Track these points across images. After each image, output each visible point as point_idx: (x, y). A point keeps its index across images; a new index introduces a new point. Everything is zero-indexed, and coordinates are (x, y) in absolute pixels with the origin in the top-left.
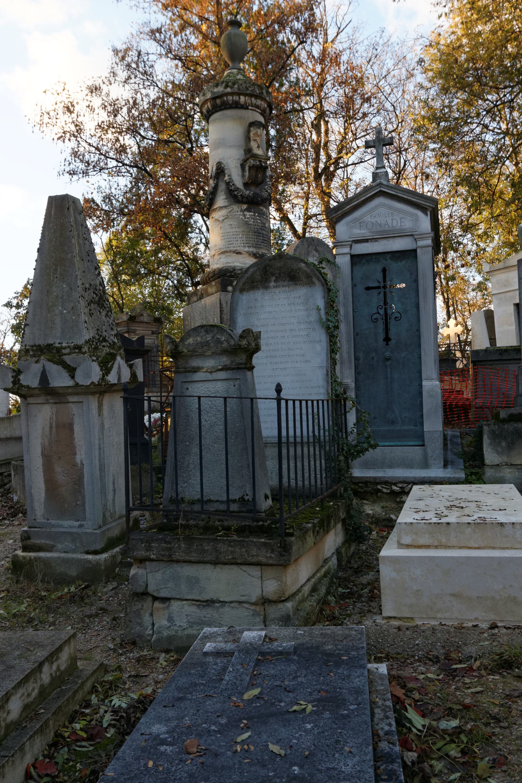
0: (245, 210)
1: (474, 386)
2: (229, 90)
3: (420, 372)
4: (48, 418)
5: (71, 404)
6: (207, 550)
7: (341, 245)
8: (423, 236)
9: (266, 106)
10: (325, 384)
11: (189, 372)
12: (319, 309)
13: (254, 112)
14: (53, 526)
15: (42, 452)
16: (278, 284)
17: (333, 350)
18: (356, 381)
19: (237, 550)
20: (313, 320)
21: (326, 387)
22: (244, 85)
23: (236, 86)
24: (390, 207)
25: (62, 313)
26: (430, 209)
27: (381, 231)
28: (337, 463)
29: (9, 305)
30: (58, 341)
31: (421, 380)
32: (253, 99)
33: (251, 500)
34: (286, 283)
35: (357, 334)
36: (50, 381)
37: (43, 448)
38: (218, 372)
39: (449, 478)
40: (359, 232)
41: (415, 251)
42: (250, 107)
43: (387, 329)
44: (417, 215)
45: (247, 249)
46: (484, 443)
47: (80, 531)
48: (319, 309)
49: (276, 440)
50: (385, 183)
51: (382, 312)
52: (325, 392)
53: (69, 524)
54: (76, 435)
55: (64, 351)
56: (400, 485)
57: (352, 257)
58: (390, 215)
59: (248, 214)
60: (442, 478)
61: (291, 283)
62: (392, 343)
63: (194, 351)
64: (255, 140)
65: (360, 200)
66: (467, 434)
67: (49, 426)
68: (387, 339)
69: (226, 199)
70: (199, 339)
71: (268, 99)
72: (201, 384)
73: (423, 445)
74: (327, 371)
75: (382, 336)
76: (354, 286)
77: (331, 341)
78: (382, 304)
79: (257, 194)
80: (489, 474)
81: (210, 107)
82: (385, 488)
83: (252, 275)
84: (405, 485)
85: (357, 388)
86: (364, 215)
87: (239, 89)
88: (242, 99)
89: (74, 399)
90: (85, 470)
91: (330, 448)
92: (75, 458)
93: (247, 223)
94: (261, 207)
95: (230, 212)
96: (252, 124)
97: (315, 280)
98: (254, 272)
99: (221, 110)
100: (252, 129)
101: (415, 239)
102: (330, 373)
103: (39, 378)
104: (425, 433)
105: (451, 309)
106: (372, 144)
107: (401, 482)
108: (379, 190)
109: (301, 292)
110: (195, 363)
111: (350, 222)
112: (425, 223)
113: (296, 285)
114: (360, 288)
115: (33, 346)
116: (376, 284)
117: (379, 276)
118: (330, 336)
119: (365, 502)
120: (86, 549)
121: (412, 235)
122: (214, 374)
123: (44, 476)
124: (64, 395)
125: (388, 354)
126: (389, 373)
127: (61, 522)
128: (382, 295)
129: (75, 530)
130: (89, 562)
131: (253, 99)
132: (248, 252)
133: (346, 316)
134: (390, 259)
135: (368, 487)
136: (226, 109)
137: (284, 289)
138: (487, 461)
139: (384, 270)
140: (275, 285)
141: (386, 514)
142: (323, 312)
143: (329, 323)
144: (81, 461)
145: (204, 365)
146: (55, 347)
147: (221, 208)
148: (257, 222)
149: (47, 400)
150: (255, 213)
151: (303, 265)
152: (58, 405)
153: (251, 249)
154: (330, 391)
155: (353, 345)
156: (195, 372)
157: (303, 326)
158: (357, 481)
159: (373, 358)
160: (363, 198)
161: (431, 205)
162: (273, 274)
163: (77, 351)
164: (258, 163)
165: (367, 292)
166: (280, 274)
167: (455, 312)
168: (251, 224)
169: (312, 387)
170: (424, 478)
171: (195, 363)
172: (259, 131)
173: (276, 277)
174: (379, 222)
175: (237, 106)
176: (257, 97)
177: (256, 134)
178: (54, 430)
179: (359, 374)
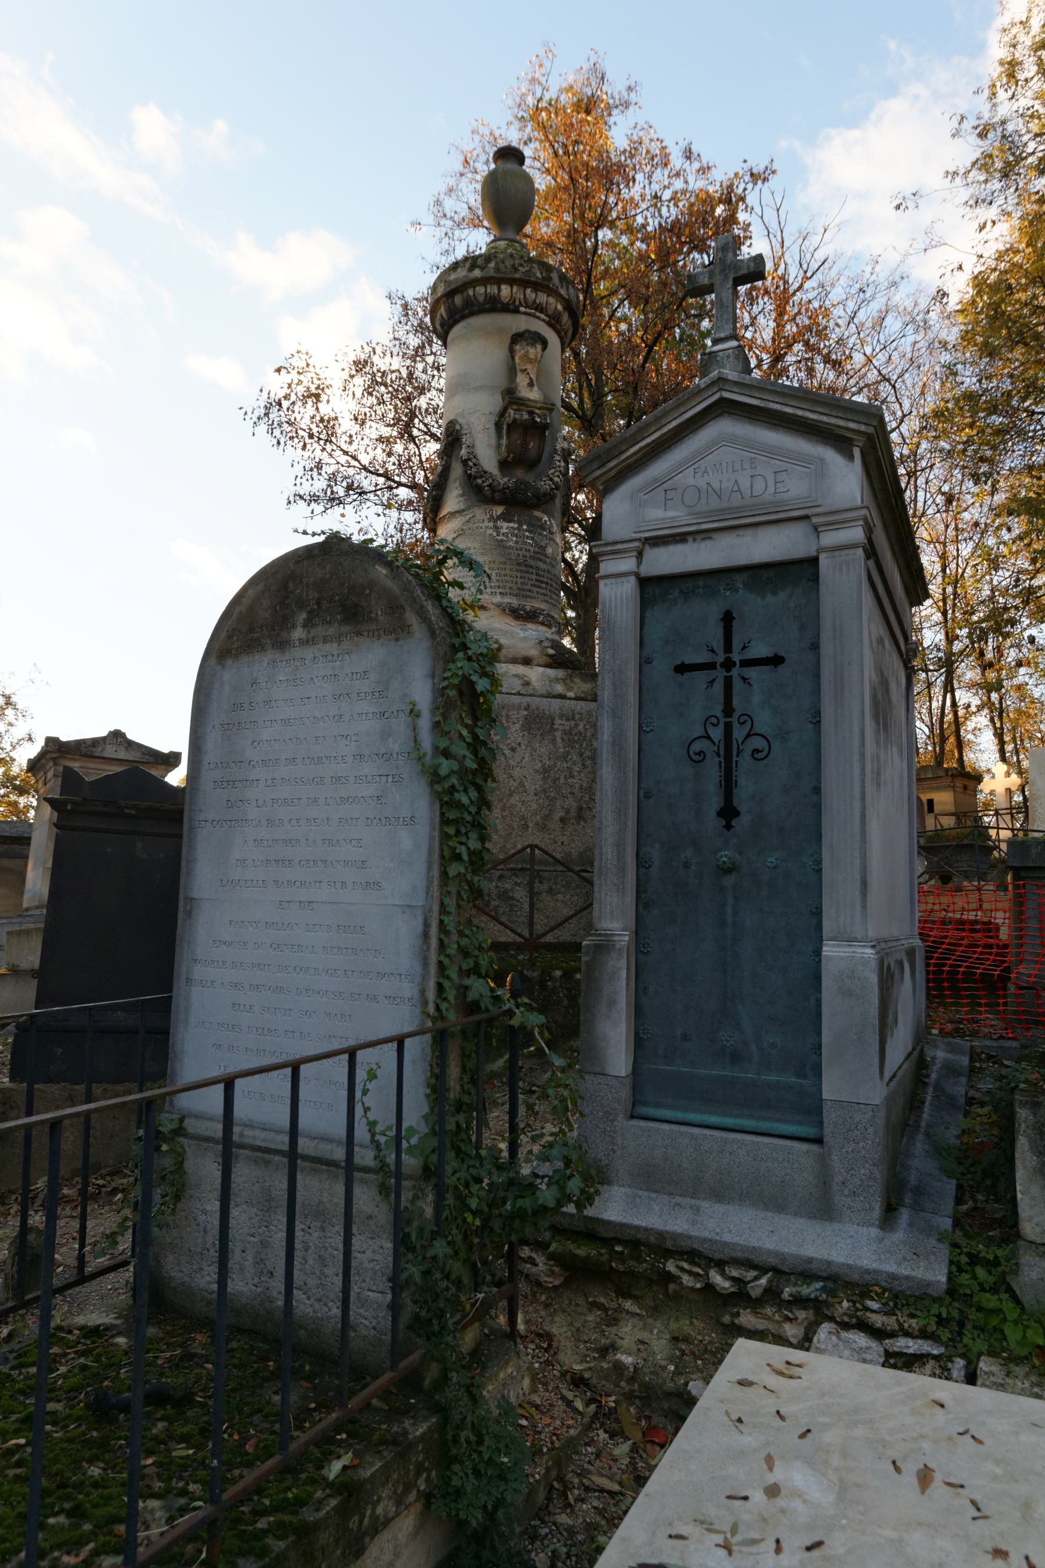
0: (499, 518)
1: (1017, 929)
2: (477, 273)
3: (817, 913)
7: (613, 552)
8: (837, 519)
9: (560, 307)
10: (418, 969)
12: (414, 713)
13: (532, 319)
21: (418, 979)
22: (509, 263)
23: (492, 265)
24: (748, 445)
26: (861, 441)
27: (722, 510)
31: (821, 939)
32: (528, 291)
34: (332, 631)
35: (647, 796)
39: (893, 1277)
40: (661, 515)
41: (813, 562)
42: (522, 309)
43: (728, 785)
44: (822, 460)
45: (498, 599)
46: (1019, 1164)
48: (414, 713)
50: (731, 374)
51: (717, 734)
56: (735, 1273)
58: (747, 466)
59: (504, 526)
60: (868, 1272)
61: (345, 629)
62: (743, 822)
64: (523, 371)
65: (665, 430)
66: (990, 1057)
68: (728, 813)
69: (462, 495)
71: (563, 292)
73: (819, 1141)
74: (427, 925)
75: (714, 802)
76: (644, 662)
78: (718, 711)
79: (526, 484)
80: (1034, 1275)
82: (690, 1273)
84: (753, 1273)
86: (678, 470)
87: (497, 269)
88: (505, 290)
93: (500, 545)
94: (536, 513)
95: (468, 521)
96: (517, 338)
99: (464, 317)
101: (816, 528)
102: (434, 931)
104: (826, 1107)
105: (1009, 747)
106: (705, 280)
107: (737, 1262)
108: (717, 396)
109: (371, 655)
111: (640, 490)
112: (846, 481)
113: (359, 634)
114: (662, 668)
116: (703, 658)
117: (715, 634)
119: (628, 1305)
121: (806, 517)
125: (726, 856)
126: (729, 910)
128: (719, 687)
131: (528, 291)
132: (499, 606)
133: (618, 742)
135: (639, 1259)
136: (472, 314)
137: (327, 647)
138: (1029, 1229)
139: (728, 619)
140: (303, 636)
141: (677, 1373)
142: (425, 723)
147: (453, 514)
148: (525, 543)
150: (520, 524)
153: (507, 600)
154: (431, 995)
157: (368, 768)
158: (610, 1235)
159: (687, 865)
160: (674, 424)
161: (863, 428)
162: (301, 605)
164: (526, 416)
165: (680, 678)
166: (318, 604)
167: (1017, 753)
168: (510, 547)
169: (381, 975)
170: (810, 1260)
172: (532, 351)
173: (310, 613)
174: (716, 485)
175: (494, 306)
176: (537, 286)
177: (526, 358)
179: (646, 906)
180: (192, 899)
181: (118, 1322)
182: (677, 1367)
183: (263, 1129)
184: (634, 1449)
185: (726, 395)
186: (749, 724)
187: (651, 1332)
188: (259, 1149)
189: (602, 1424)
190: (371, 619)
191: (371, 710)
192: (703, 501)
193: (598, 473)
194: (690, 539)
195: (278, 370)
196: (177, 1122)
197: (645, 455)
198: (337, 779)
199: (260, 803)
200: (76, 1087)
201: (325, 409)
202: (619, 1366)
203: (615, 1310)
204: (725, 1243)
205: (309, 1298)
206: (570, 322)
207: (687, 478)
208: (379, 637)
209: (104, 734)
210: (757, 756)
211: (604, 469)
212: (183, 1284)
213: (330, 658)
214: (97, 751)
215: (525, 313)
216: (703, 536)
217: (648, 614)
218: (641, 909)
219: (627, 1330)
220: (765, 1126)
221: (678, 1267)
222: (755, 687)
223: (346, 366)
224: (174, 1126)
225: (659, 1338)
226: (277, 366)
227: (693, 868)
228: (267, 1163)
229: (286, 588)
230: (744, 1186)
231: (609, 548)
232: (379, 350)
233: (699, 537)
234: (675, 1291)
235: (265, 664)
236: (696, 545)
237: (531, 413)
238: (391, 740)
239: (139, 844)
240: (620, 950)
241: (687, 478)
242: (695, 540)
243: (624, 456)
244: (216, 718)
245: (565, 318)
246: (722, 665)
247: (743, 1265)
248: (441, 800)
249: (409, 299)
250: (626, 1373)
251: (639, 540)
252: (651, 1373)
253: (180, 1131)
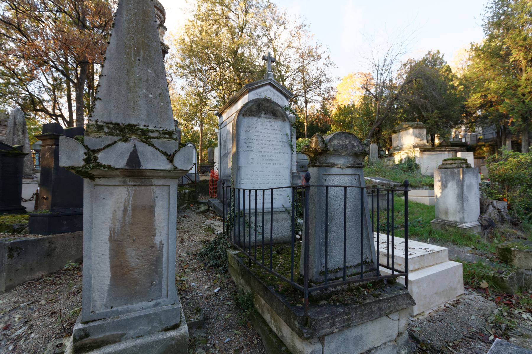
4: (123, 201)
5: (154, 187)
6: (375, 311)
11: (328, 166)
14: (121, 313)
15: (110, 236)
19: (392, 304)
24: (273, 92)
25: (147, 97)
30: (144, 124)
33: (370, 261)
34: (270, 117)
36: (142, 163)
37: (113, 232)
38: (347, 169)
47: (158, 310)
49: (270, 210)
53: (141, 307)
54: (156, 217)
55: (151, 134)
63: (337, 151)
67: (123, 208)
70: (341, 142)
72: (335, 177)
83: (251, 107)
89: (161, 182)
90: (165, 250)
92: (154, 239)
103: (126, 159)
110: (332, 160)
115: (107, 123)
120: (164, 327)
122: (344, 169)
123: (111, 262)
124: (149, 178)
127: (131, 307)
129: (152, 311)
130: (173, 338)
144: (161, 242)
145: (338, 163)
146: (139, 129)
149: (125, 182)
152: (137, 188)
156: (333, 167)
157: (279, 144)
163: (167, 136)
171: (332, 160)
178: (129, 213)
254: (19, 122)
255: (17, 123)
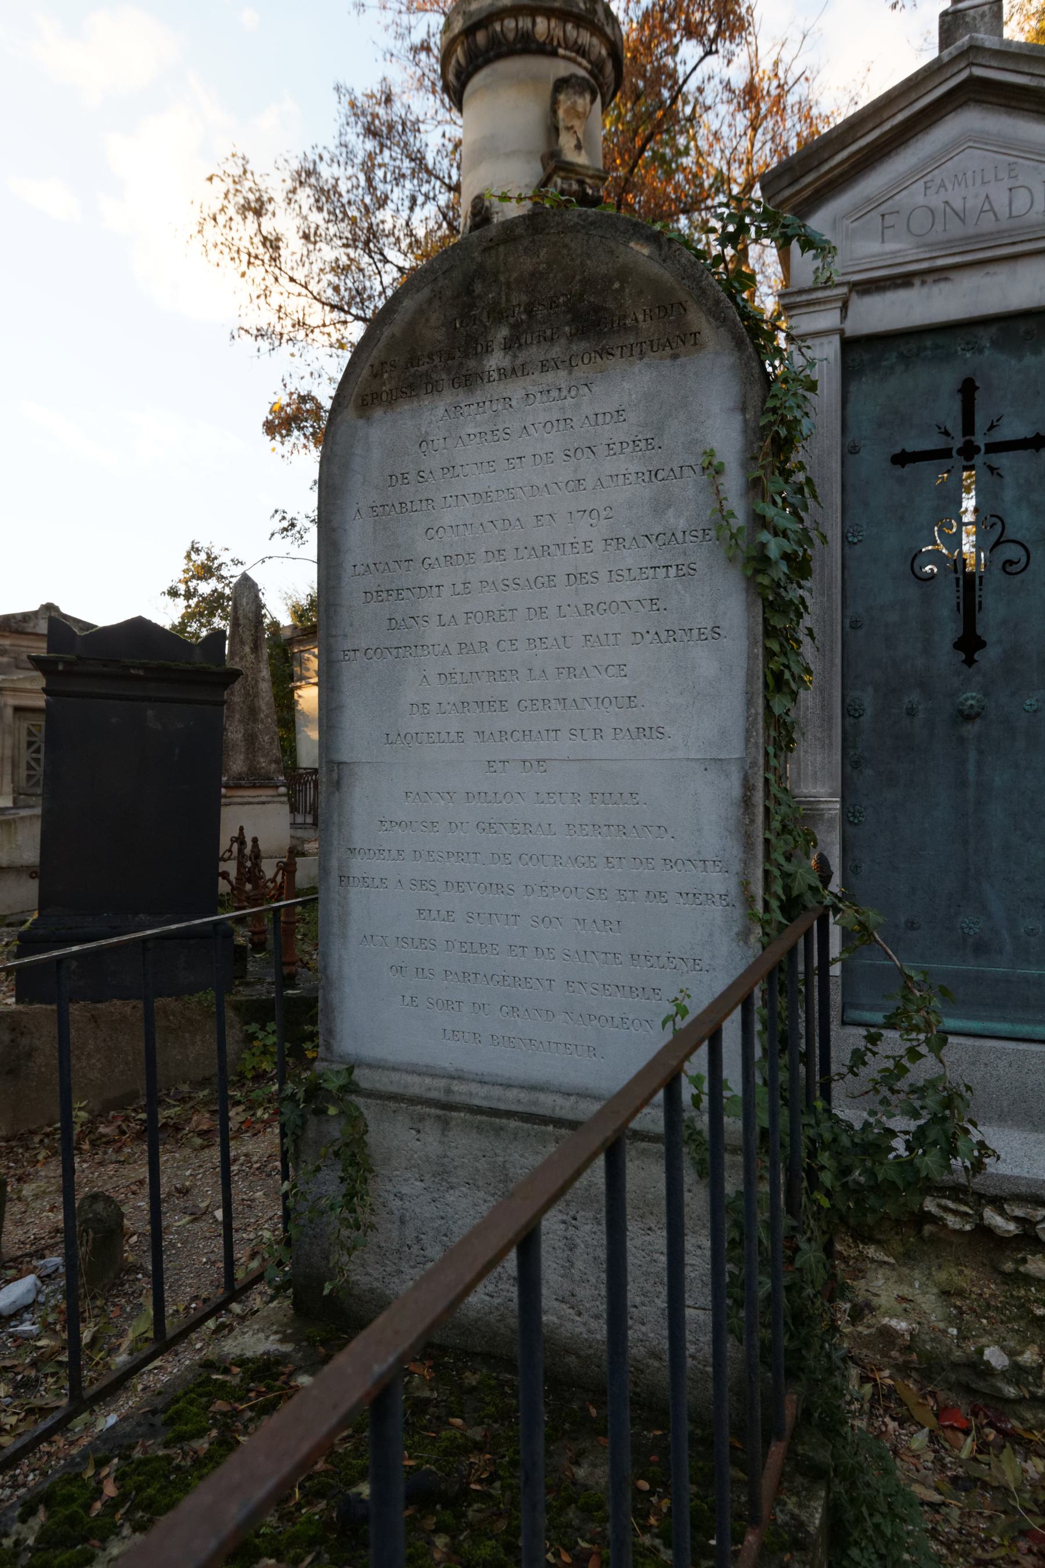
9: (604, 52)
10: (734, 851)
12: (713, 469)
16: (522, 356)
17: (778, 676)
18: (847, 790)
20: (682, 524)
21: (736, 867)
24: (1006, 145)
27: (966, 239)
28: (786, 1280)
29: (173, 593)
32: (569, 27)
34: (556, 351)
35: (855, 625)
52: (734, 890)
56: (1019, 1212)
57: (850, 345)
58: (1003, 174)
62: (989, 657)
64: (569, 128)
65: (887, 126)
68: (970, 644)
74: (748, 787)
75: (950, 630)
76: (850, 451)
77: (769, 631)
81: (462, 60)
82: (955, 1213)
85: (849, 817)
86: (901, 185)
91: (748, 1182)
96: (562, 84)
97: (698, 319)
98: (420, 312)
99: (488, 62)
100: (562, 97)
102: (759, 796)
109: (626, 387)
111: (845, 216)
114: (873, 458)
117: (950, 411)
118: (769, 606)
119: (871, 1251)
125: (971, 698)
126: (971, 767)
134: (995, 343)
136: (500, 56)
137: (550, 377)
139: (968, 389)
141: (962, 1337)
142: (733, 482)
143: (765, 536)
151: (642, 250)
154: (758, 890)
155: (838, 661)
157: (630, 558)
159: (911, 712)
160: (900, 117)
162: (498, 315)
164: (575, 187)
165: (899, 471)
166: (530, 312)
172: (580, 102)
173: (515, 327)
174: (958, 204)
175: (528, 46)
177: (573, 111)
179: (856, 765)
180: (340, 763)
181: (287, 1348)
182: (959, 1329)
183: (482, 1082)
184: (933, 1438)
185: (978, 72)
186: (999, 528)
187: (911, 1285)
188: (478, 1110)
189: (887, 1409)
190: (626, 328)
191: (632, 469)
192: (939, 227)
193: (787, 193)
194: (917, 282)
195: (210, 179)
196: (345, 1074)
197: (853, 166)
198: (576, 577)
199: (445, 619)
200: (99, 1005)
201: (268, 225)
202: (887, 1334)
203: (856, 1259)
204: (1004, 1176)
205: (579, 1314)
206: (613, 76)
207: (915, 196)
208: (642, 355)
209: (36, 608)
210: (1009, 569)
211: (797, 187)
212: (372, 1291)
213: (554, 393)
214: (29, 627)
215: (564, 57)
216: (936, 276)
217: (853, 388)
218: (849, 769)
219: (881, 1282)
220: (1024, 1029)
221: (939, 1206)
222: (1008, 479)
223: (287, 176)
224: (341, 1081)
225: (925, 1293)
226: (208, 175)
227: (921, 715)
228: (498, 1131)
229: (469, 292)
230: (1005, 1103)
231: (804, 297)
232: (326, 156)
233: (929, 279)
234: (932, 1234)
235: (441, 411)
236: (925, 290)
237: (581, 183)
238: (671, 512)
239: (150, 713)
240: (832, 820)
241: (915, 196)
242: (923, 283)
243: (826, 167)
244: (361, 495)
245: (609, 67)
246: (960, 452)
247: (1030, 1202)
248: (765, 599)
249: (358, 93)
250: (899, 1341)
251: (848, 283)
252: (932, 1340)
253: (350, 1088)
254: (245, 617)
255: (242, 621)
